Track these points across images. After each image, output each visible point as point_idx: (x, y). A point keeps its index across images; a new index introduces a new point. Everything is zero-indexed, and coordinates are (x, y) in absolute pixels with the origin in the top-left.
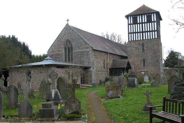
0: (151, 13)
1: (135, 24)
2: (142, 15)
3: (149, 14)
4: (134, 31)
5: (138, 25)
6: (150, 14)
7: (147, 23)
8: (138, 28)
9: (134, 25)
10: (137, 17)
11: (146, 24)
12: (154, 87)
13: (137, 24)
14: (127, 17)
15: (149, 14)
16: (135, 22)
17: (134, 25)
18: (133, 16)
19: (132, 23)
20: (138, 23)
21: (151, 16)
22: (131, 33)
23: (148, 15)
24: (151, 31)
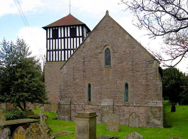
0: (76, 26)
1: (73, 38)
2: (64, 27)
3: (55, 28)
4: (51, 49)
5: (60, 40)
6: (74, 27)
7: (52, 39)
8: (59, 44)
9: (72, 39)
10: (76, 27)
11: (69, 39)
12: (169, 127)
13: (77, 37)
14: (46, 28)
15: (73, 26)
16: (55, 36)
17: (54, 40)
18: (52, 27)
19: (51, 37)
20: (60, 38)
21: (58, 30)
22: (50, 51)
23: (72, 27)
24: (57, 50)
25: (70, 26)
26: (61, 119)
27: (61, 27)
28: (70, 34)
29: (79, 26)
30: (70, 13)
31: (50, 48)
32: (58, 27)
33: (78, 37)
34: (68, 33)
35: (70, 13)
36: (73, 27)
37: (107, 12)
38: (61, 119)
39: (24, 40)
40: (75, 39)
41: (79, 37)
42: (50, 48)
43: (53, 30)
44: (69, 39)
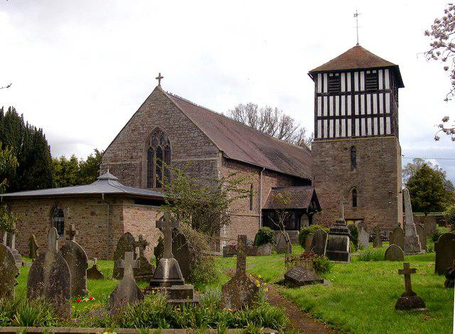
5: (343, 97)
7: (365, 93)
8: (342, 105)
10: (378, 73)
15: (371, 69)
16: (334, 90)
17: (331, 98)
18: (328, 72)
20: (343, 94)
21: (339, 78)
22: (323, 118)
23: (368, 72)
24: (337, 118)
25: (365, 70)
26: (175, 229)
27: (346, 72)
28: (328, 88)
29: (383, 69)
30: (358, 44)
31: (360, 112)
32: (340, 72)
33: (343, 94)
34: (360, 82)
35: (358, 44)
36: (334, 75)
37: (160, 78)
38: (175, 229)
39: (24, 116)
40: (337, 97)
41: (346, 94)
42: (360, 112)
43: (330, 78)
44: (325, 98)
